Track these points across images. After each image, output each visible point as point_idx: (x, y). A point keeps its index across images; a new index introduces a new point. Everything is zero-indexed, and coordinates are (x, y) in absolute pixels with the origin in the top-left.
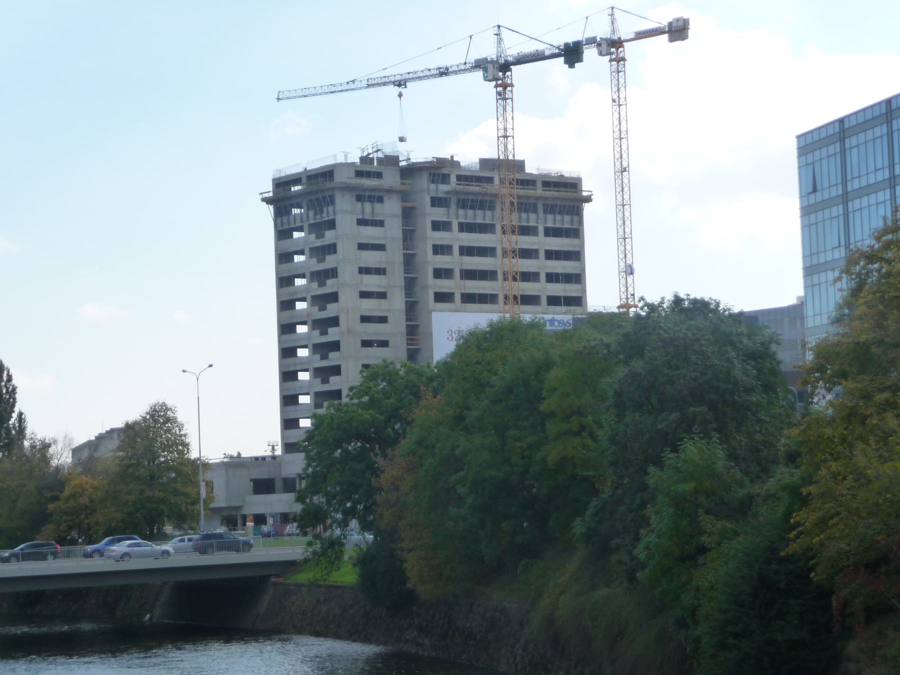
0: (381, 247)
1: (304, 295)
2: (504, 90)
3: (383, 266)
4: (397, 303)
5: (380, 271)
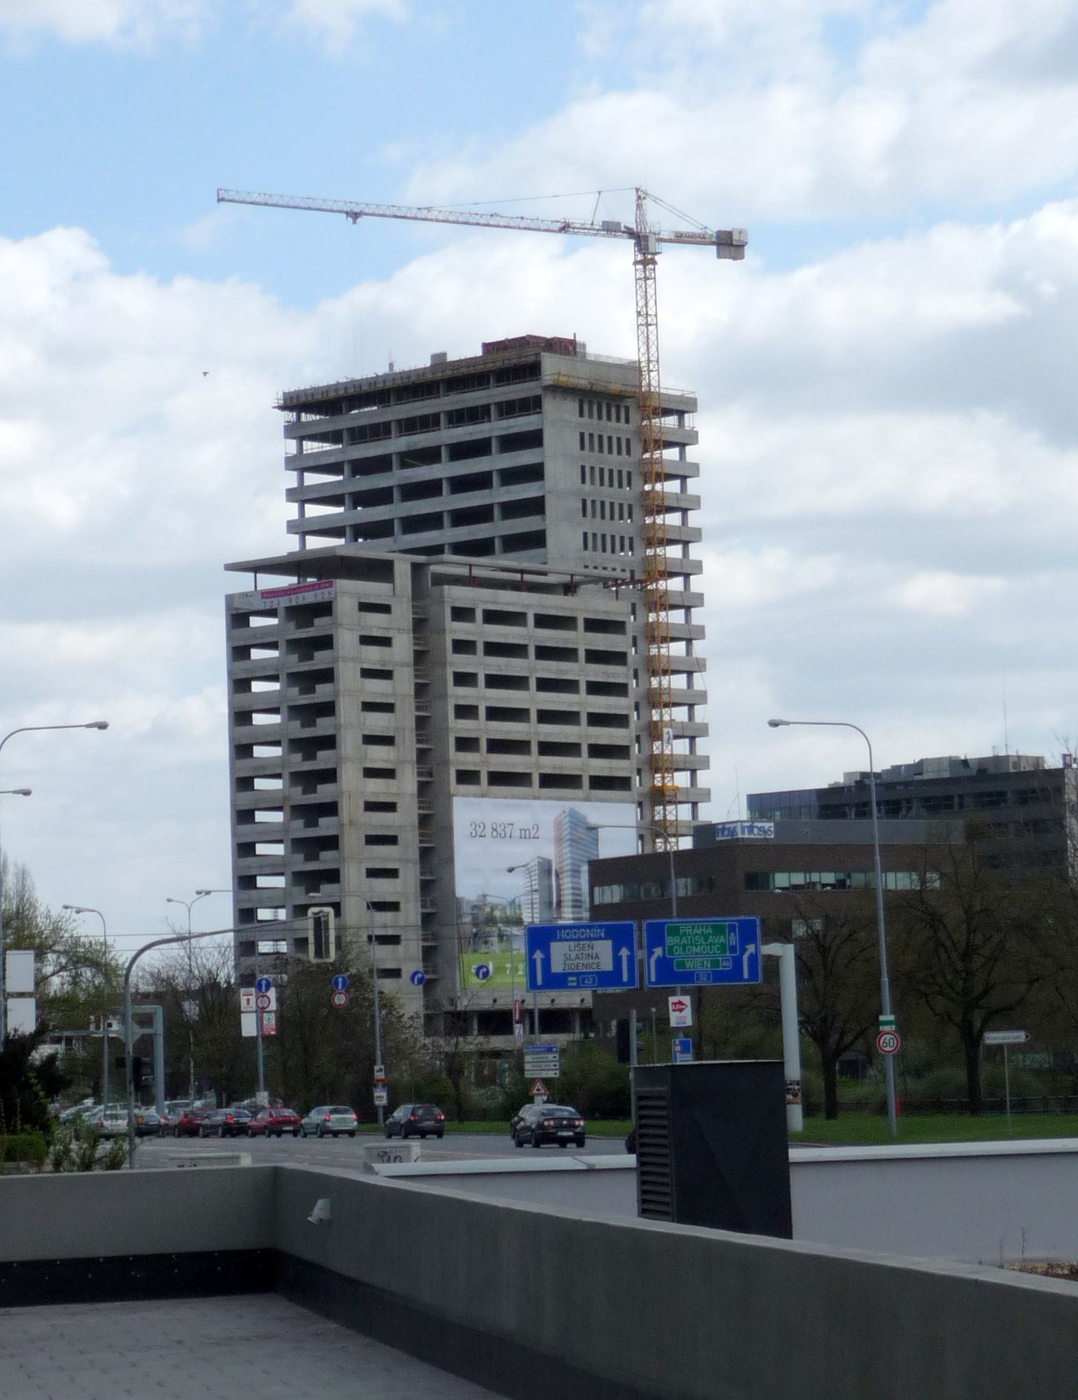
0: (388, 708)
1: (278, 771)
2: (646, 260)
3: (391, 734)
4: (407, 784)
5: (387, 741)
